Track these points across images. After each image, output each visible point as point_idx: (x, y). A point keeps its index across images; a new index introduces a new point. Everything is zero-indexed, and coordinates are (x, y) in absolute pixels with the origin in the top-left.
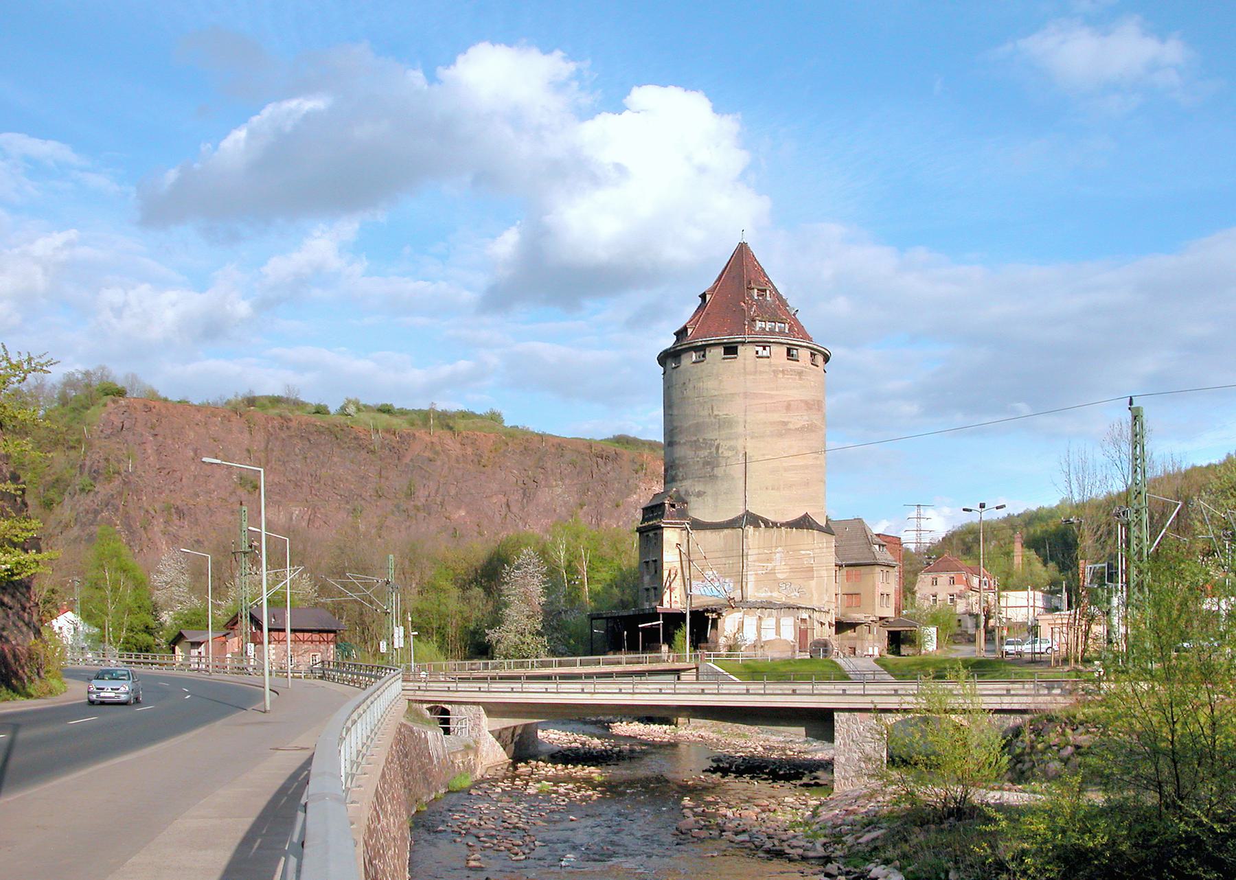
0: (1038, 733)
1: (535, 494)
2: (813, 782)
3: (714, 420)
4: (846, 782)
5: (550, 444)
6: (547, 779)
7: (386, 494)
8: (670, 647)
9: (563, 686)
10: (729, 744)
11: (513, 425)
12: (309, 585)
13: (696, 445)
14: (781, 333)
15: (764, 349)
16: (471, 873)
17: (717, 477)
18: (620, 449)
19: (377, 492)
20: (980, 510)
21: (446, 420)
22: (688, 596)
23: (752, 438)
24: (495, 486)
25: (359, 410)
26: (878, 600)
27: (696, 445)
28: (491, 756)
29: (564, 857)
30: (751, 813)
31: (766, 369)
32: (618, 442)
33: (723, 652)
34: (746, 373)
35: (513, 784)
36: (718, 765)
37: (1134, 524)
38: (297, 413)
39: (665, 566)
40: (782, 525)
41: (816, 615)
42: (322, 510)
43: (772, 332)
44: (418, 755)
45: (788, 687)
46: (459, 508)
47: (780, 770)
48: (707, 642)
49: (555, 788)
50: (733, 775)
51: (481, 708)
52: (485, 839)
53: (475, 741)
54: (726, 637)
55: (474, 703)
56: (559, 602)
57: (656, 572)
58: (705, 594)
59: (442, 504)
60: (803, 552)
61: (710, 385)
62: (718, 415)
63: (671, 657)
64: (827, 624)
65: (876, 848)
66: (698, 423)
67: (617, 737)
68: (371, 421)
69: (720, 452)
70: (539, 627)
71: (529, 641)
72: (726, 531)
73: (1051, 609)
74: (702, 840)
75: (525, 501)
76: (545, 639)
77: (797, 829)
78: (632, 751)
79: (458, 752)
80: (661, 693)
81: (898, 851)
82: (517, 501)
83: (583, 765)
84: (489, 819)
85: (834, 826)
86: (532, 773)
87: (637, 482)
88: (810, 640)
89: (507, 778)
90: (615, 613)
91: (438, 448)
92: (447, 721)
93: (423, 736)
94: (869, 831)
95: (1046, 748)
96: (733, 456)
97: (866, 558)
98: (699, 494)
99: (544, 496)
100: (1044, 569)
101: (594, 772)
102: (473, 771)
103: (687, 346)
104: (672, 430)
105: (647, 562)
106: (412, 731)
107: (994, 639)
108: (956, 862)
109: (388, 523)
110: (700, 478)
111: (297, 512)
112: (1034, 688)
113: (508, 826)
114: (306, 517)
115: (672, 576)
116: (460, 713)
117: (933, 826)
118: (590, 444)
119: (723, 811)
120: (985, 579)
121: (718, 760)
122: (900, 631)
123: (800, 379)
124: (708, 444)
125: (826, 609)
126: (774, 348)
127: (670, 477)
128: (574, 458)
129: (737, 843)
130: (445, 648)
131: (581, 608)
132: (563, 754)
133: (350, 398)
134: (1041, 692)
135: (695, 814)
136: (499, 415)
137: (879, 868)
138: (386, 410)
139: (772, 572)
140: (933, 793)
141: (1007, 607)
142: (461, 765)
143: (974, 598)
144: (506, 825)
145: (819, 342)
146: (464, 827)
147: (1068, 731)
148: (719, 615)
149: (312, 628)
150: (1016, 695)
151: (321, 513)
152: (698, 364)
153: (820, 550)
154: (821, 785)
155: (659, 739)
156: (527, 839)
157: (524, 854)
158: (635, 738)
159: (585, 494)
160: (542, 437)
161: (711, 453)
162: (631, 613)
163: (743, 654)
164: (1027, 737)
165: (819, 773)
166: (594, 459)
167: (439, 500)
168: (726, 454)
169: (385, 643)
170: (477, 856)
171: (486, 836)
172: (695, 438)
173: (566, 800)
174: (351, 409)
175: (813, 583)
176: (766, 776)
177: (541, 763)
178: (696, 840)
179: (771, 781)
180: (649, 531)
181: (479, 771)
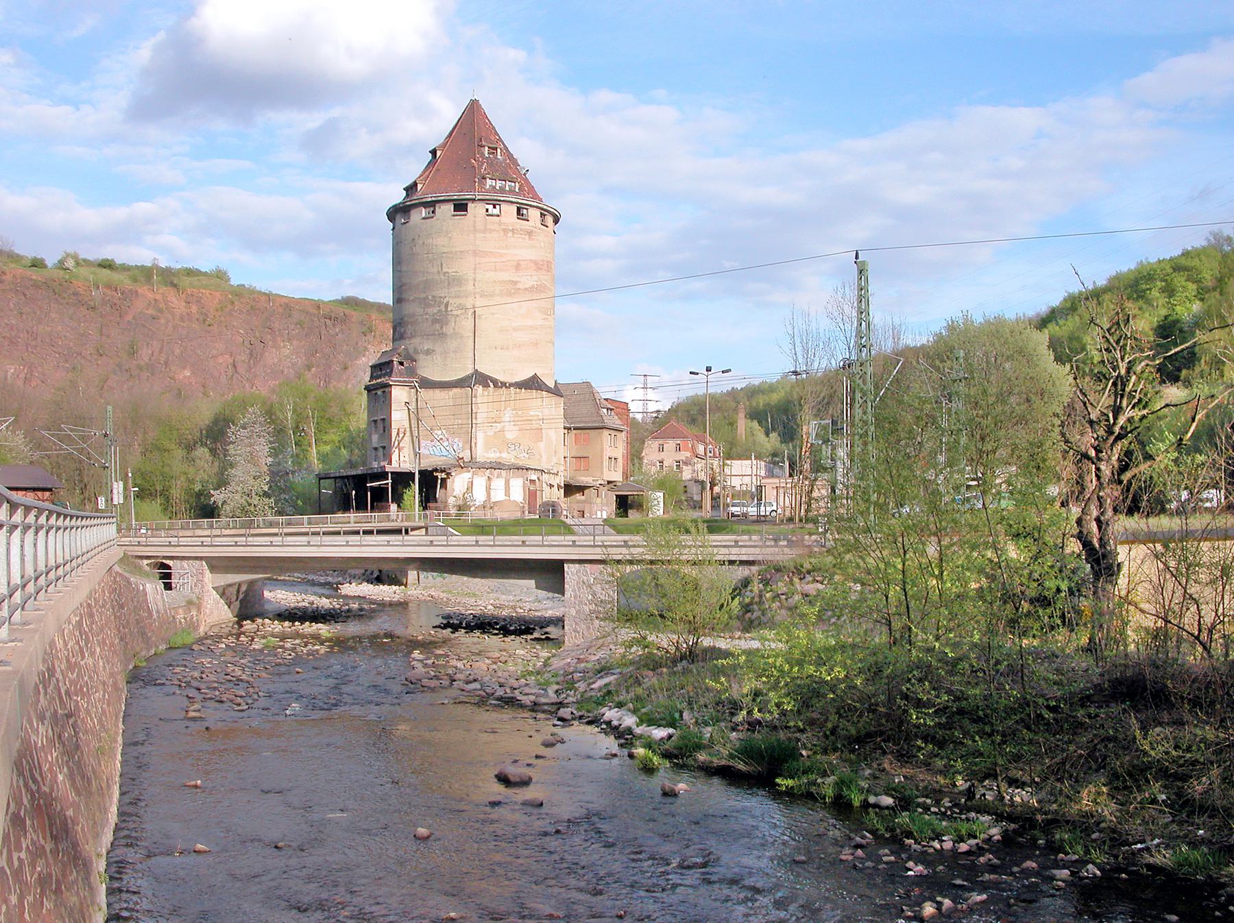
0: (766, 582)
1: (262, 355)
2: (543, 637)
3: (442, 277)
4: (573, 636)
5: (278, 304)
6: (273, 636)
7: (106, 352)
8: (399, 506)
10: (459, 603)
11: (239, 283)
12: (24, 442)
13: (425, 302)
14: (512, 191)
15: (494, 207)
16: (191, 724)
19: (98, 351)
20: (706, 373)
21: (169, 277)
22: (417, 454)
23: (481, 297)
25: (78, 264)
26: (606, 463)
27: (425, 302)
28: (216, 613)
29: (289, 706)
30: (482, 665)
32: (346, 304)
33: (453, 511)
35: (238, 640)
36: (449, 622)
37: (859, 376)
38: (13, 266)
40: (511, 385)
41: (545, 477)
42: (40, 369)
43: (502, 190)
44: (135, 607)
45: (518, 539)
46: (184, 368)
47: (511, 626)
48: (436, 502)
49: (281, 644)
50: (463, 631)
51: (204, 563)
52: (207, 691)
53: (198, 598)
54: (455, 497)
55: (196, 558)
56: (287, 462)
57: (384, 431)
58: (433, 455)
59: (166, 364)
61: (440, 242)
62: (448, 273)
63: (400, 517)
64: (556, 486)
65: (609, 692)
66: (427, 280)
67: (346, 597)
68: (92, 276)
69: (449, 309)
70: (266, 488)
71: (256, 503)
72: (455, 390)
73: (770, 474)
74: (433, 690)
75: (252, 362)
76: (272, 500)
77: (528, 678)
78: (361, 610)
79: (180, 607)
80: (388, 545)
81: (632, 695)
82: (243, 361)
83: (311, 622)
84: (211, 673)
85: (566, 674)
86: (258, 631)
87: (366, 344)
89: (232, 635)
90: (344, 473)
91: (162, 305)
92: (168, 576)
93: (141, 588)
94: (602, 677)
95: (774, 597)
97: (595, 421)
98: (428, 352)
99: (271, 357)
100: (767, 439)
101: (323, 629)
102: (196, 628)
103: (417, 201)
104: (401, 287)
105: (375, 421)
106: (129, 582)
107: (719, 506)
108: (690, 703)
109: (110, 382)
111: (12, 371)
112: (761, 539)
113: (232, 678)
114: (22, 376)
115: (401, 435)
116: (182, 568)
117: (665, 670)
118: (318, 305)
119: (454, 663)
120: (710, 446)
121: (448, 617)
122: (627, 496)
123: (530, 239)
124: (437, 301)
126: (504, 206)
127: (399, 333)
128: (303, 318)
129: (467, 692)
130: (168, 508)
131: (309, 469)
132: (290, 613)
133: (69, 251)
134: (768, 543)
135: (426, 666)
136: (225, 273)
137: (612, 711)
138: (107, 265)
140: (664, 640)
141: (731, 476)
142: (183, 620)
143: (700, 465)
144: (229, 677)
145: (550, 203)
146: (185, 680)
147: (796, 580)
148: (449, 474)
149: (26, 486)
150: (744, 546)
151: (38, 372)
152: (427, 220)
153: (550, 410)
154: (553, 639)
155: (388, 599)
156: (251, 690)
157: (247, 704)
158: (365, 597)
159: (313, 355)
160: (269, 296)
162: (360, 472)
163: (473, 515)
164: (756, 587)
165: (548, 629)
166: (323, 320)
167: (162, 360)
169: (103, 499)
170: (196, 706)
171: (208, 688)
172: (423, 295)
173: (293, 654)
174: (70, 264)
175: (542, 445)
176: (497, 632)
177: (267, 621)
178: (426, 689)
179: (501, 636)
180: (377, 389)
181: (202, 627)
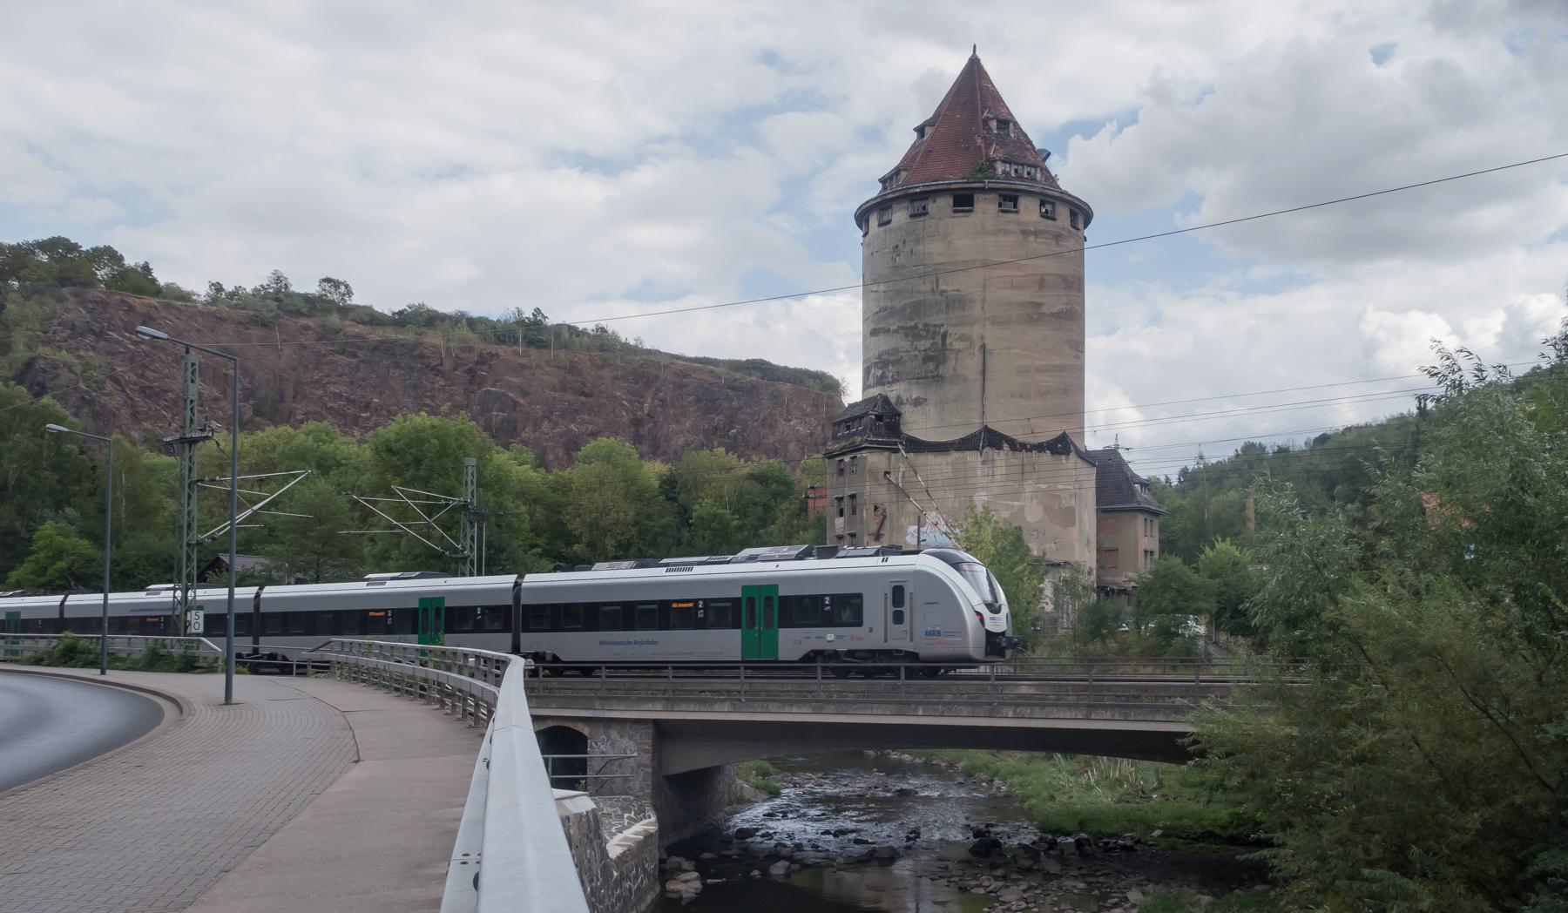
3: (938, 297)
69: (948, 341)
161: (934, 344)
172: (912, 324)
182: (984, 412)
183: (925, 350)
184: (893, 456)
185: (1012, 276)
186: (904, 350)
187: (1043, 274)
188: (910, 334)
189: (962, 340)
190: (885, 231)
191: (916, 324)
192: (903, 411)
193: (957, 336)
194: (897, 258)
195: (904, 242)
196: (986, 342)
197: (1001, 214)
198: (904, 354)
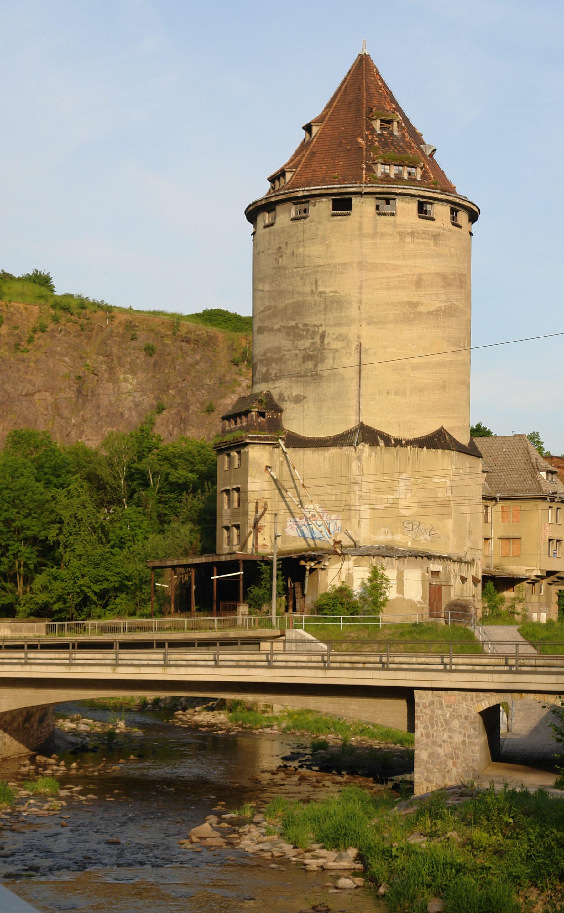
3: (317, 298)
9: (78, 656)
14: (412, 181)
17: (321, 376)
18: (212, 330)
24: (39, 379)
31: (389, 229)
34: (361, 235)
39: (251, 496)
43: (399, 178)
60: (436, 480)
64: (470, 580)
69: (326, 341)
88: (445, 602)
96: (343, 348)
98: (298, 400)
110: (300, 376)
115: (260, 511)
123: (436, 244)
125: (469, 558)
139: (395, 506)
161: (313, 344)
168: (335, 345)
172: (293, 323)
182: (360, 409)
183: (305, 349)
184: (276, 450)
185: (389, 277)
186: (286, 348)
187: (421, 274)
188: (292, 334)
189: (339, 340)
190: (270, 233)
191: (297, 324)
192: (284, 408)
193: (334, 337)
194: (280, 260)
195: (287, 244)
196: (362, 342)
197: (378, 217)
198: (285, 353)
